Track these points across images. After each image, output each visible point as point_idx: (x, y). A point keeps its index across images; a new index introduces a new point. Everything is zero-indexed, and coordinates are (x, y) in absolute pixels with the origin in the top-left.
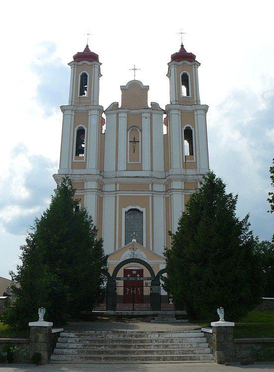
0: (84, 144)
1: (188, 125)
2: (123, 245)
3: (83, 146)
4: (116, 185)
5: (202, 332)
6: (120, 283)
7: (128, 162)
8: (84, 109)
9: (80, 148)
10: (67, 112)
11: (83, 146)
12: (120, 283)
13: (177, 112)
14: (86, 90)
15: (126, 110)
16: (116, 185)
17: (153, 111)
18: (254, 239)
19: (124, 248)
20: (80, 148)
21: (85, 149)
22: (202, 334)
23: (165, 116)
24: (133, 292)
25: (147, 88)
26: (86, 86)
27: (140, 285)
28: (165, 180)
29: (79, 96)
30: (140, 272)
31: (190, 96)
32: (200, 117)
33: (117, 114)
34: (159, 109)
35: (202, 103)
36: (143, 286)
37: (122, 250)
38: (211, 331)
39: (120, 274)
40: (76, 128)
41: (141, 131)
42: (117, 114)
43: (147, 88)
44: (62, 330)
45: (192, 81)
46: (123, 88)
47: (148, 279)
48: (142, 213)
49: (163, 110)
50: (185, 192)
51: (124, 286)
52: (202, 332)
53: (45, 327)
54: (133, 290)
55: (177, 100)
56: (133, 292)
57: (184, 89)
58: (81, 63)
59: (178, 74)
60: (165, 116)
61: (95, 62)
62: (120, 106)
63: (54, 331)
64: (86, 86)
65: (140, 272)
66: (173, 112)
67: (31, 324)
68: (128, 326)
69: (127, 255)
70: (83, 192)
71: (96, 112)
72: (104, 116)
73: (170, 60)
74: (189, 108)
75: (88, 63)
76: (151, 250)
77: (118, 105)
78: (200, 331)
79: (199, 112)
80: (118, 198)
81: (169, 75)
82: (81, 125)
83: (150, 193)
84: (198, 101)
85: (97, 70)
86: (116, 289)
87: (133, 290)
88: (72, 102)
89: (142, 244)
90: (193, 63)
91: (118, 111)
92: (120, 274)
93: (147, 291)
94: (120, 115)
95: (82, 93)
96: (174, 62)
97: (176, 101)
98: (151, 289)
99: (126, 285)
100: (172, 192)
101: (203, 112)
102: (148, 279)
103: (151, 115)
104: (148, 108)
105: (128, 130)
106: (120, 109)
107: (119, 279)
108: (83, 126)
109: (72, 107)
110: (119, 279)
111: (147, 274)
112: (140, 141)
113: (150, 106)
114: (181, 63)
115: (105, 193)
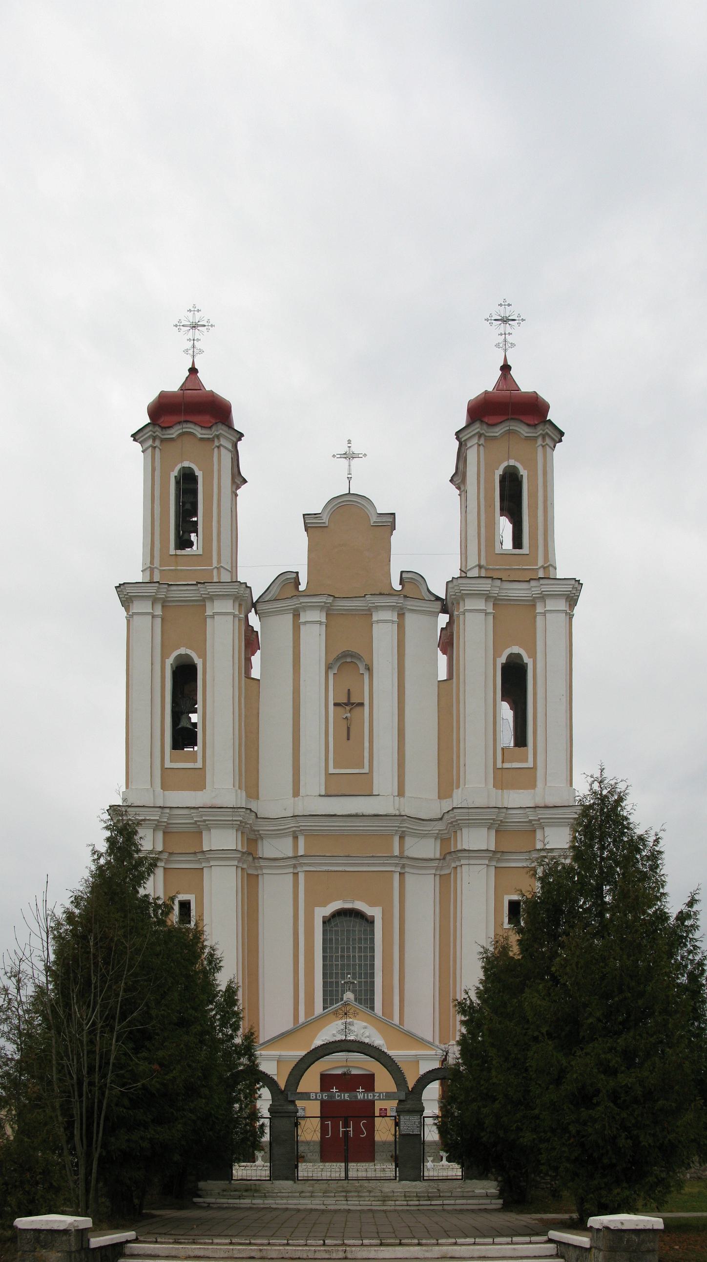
0: (195, 711)
1: (516, 650)
2: (319, 1009)
3: (194, 718)
4: (296, 838)
5: (550, 1241)
6: (310, 1109)
7: (332, 770)
8: (190, 594)
9: (183, 724)
10: (137, 607)
11: (194, 718)
12: (310, 1109)
13: (480, 604)
14: (196, 532)
15: (323, 599)
16: (296, 838)
17: (410, 604)
18: (502, 1120)
19: (321, 1017)
20: (183, 724)
21: (199, 730)
22: (551, 1248)
23: (443, 619)
24: (346, 1133)
25: (389, 522)
26: (195, 519)
27: (367, 1111)
28: (440, 826)
29: (172, 551)
30: (368, 1081)
31: (525, 550)
32: (555, 622)
33: (296, 615)
34: (427, 596)
35: (561, 573)
36: (373, 1117)
37: (315, 1023)
38: (583, 1240)
39: (310, 1082)
40: (170, 661)
41: (369, 669)
42: (296, 615)
43: (389, 522)
44: (131, 1234)
45: (533, 495)
46: (311, 523)
47: (389, 1096)
48: (373, 922)
49: (438, 598)
50: (499, 860)
51: (323, 1117)
52: (550, 1241)
53: (65, 1232)
54: (346, 1125)
55: (483, 563)
56: (346, 1133)
57: (505, 526)
58: (174, 432)
59: (490, 471)
60: (443, 619)
61: (221, 430)
62: (302, 587)
63: (96, 1241)
64: (195, 519)
65: (368, 1081)
66: (470, 604)
67: (23, 1222)
68: (195, 1203)
69: (330, 1032)
70: (199, 861)
71: (228, 606)
72: (254, 620)
73: (461, 420)
74: (518, 591)
75: (198, 432)
76: (396, 1021)
77: (297, 583)
78: (545, 1238)
79: (551, 604)
80: (301, 876)
81: (459, 479)
82: (182, 651)
83: (396, 865)
84: (549, 566)
85: (226, 457)
86: (296, 1125)
87: (346, 1125)
88: (152, 570)
89: (372, 1008)
90: (540, 431)
91: (295, 601)
92: (310, 1082)
93: (384, 1131)
94: (304, 617)
95: (183, 543)
96: (477, 428)
97: (480, 567)
98: (397, 1124)
99: (329, 1111)
100: (459, 859)
101: (562, 605)
102: (389, 1096)
103: (401, 616)
104: (392, 593)
105: (329, 667)
106: (305, 594)
107: (306, 1096)
108: (189, 652)
109: (152, 590)
110: (306, 1096)
111: (384, 1082)
112: (367, 703)
113: (397, 586)
114: (498, 431)
115: (263, 863)
